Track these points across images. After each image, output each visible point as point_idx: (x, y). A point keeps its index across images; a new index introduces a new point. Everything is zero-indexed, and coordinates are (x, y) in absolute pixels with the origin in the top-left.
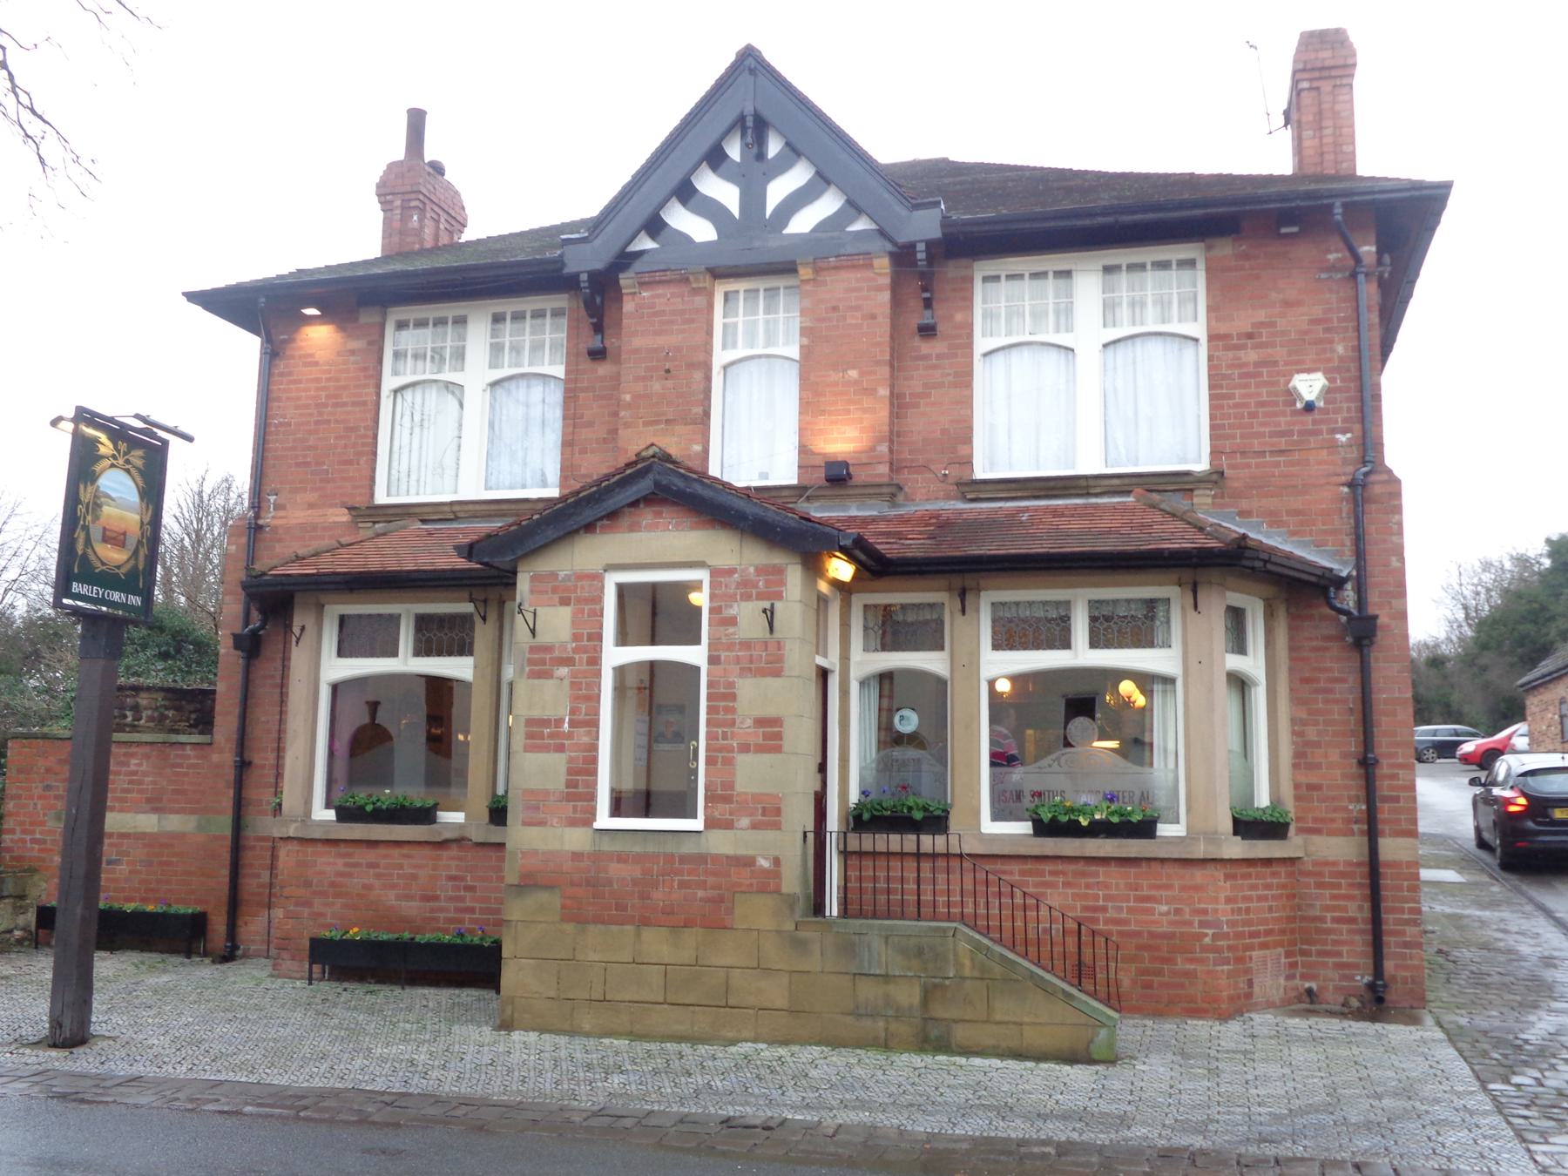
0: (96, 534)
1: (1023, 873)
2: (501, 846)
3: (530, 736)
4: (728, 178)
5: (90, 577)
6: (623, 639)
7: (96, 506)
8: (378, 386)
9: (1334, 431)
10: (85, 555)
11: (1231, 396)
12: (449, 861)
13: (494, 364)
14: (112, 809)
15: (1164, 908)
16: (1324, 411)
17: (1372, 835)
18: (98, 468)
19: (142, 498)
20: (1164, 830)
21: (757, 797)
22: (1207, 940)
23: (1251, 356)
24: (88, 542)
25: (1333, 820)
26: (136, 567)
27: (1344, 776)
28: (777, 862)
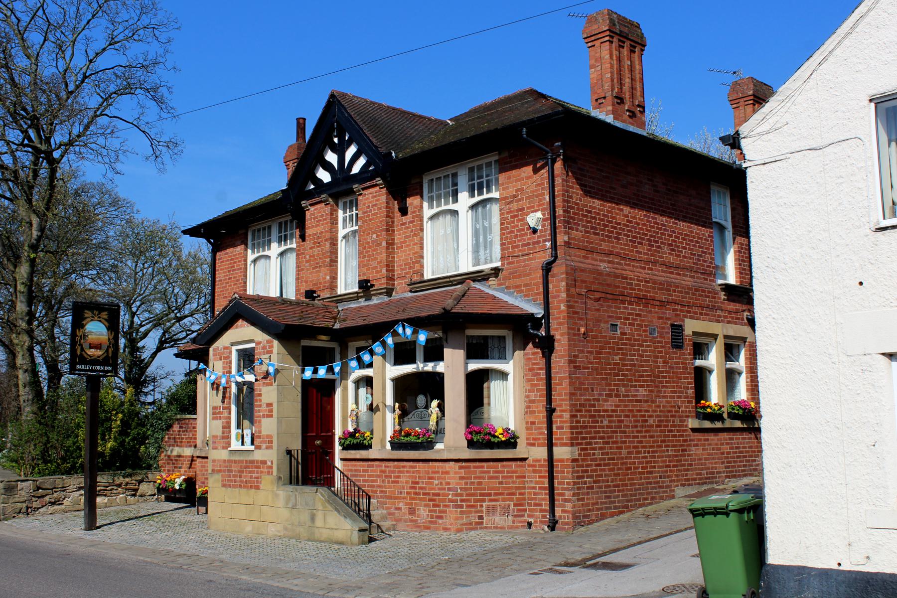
0: (86, 346)
1: (517, 466)
3: (214, 413)
5: (83, 360)
7: (85, 336)
8: (246, 260)
9: (545, 241)
10: (81, 354)
12: (377, 467)
13: (473, 196)
14: (544, 460)
16: (542, 231)
17: (550, 446)
18: (84, 322)
19: (108, 329)
22: (450, 497)
23: (514, 206)
24: (82, 350)
25: (539, 439)
26: (108, 355)
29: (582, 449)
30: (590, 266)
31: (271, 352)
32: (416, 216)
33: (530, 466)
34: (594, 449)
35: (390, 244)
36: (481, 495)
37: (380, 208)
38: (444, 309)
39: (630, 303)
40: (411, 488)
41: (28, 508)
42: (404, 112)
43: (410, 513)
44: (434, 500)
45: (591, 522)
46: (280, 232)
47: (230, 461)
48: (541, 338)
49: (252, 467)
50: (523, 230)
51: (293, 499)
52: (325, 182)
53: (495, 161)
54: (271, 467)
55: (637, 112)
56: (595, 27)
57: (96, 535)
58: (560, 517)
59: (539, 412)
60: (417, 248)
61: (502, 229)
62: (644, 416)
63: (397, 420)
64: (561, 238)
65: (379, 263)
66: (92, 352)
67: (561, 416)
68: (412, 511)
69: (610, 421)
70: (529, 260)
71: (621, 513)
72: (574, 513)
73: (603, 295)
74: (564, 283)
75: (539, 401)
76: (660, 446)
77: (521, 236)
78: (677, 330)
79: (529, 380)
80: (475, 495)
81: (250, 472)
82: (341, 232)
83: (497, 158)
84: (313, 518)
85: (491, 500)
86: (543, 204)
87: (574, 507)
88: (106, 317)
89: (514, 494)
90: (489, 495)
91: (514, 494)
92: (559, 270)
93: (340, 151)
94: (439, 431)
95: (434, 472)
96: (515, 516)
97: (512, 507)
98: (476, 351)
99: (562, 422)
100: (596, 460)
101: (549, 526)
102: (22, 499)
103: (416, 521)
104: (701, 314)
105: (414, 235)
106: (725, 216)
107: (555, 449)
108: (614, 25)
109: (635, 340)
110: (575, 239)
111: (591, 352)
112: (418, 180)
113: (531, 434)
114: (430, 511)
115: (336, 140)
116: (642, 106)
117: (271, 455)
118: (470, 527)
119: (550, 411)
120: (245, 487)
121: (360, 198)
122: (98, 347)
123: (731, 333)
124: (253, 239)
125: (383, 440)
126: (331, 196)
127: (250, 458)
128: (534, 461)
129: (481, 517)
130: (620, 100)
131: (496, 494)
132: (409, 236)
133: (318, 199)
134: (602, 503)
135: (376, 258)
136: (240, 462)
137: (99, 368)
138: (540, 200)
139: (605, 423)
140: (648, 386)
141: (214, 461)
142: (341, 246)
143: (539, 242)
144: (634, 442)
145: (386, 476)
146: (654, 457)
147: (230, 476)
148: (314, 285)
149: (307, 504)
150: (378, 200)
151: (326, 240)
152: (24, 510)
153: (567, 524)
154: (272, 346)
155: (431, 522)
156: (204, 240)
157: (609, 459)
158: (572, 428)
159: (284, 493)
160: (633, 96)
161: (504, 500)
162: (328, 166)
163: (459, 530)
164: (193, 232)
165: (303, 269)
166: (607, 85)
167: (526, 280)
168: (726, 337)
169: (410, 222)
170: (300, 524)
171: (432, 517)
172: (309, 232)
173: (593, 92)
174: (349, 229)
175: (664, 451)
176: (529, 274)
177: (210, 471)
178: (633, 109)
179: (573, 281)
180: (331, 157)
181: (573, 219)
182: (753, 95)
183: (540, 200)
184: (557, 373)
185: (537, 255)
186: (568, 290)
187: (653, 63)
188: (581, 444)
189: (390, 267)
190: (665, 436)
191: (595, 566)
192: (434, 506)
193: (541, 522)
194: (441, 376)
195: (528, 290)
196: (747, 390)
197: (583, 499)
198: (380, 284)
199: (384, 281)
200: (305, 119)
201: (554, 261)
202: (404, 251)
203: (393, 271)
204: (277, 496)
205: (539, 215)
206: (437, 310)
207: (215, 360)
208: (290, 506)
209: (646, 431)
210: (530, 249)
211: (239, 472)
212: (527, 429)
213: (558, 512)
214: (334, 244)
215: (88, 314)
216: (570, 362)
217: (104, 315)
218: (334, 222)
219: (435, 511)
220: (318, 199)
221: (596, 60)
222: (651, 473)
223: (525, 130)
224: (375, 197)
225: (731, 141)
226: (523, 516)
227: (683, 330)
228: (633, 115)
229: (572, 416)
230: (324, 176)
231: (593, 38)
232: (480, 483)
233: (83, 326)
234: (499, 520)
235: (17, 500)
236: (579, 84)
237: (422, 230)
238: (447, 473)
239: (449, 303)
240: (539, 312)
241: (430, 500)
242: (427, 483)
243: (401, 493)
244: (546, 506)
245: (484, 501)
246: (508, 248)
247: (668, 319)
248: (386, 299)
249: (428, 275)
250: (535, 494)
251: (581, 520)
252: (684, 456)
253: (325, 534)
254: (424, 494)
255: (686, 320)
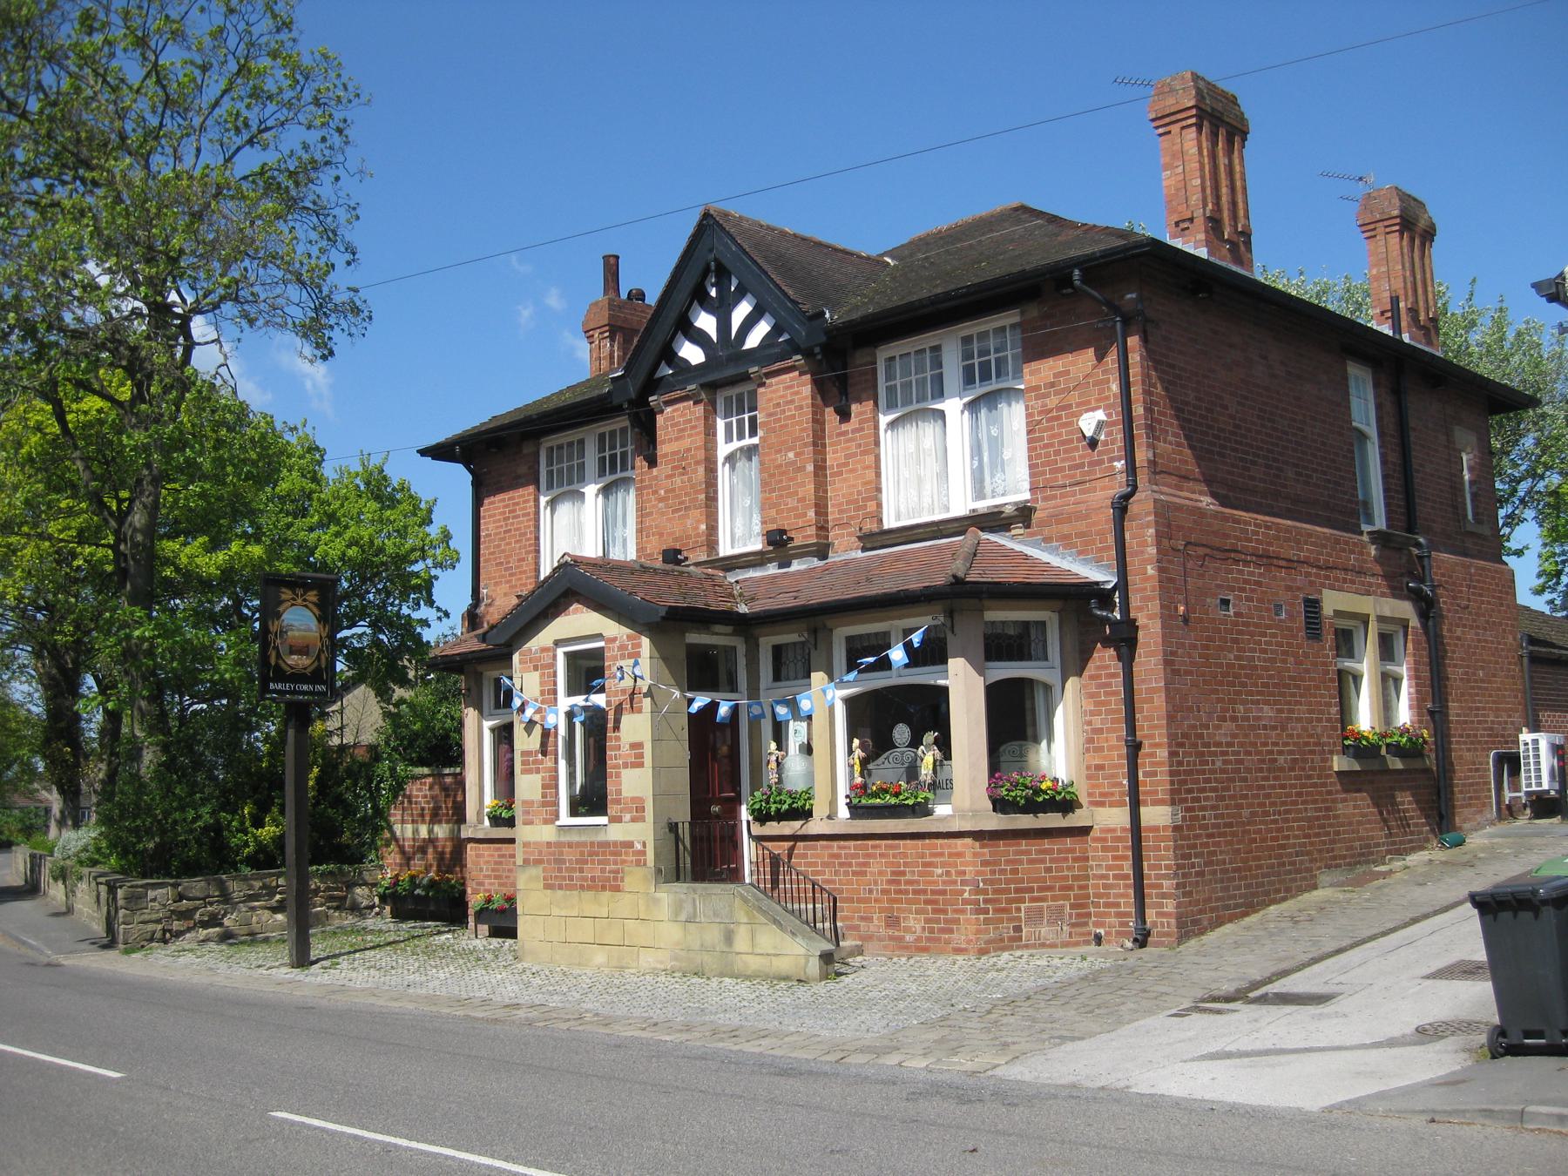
2: (512, 841)
4: (710, 311)
5: (281, 675)
6: (571, 692)
7: (283, 633)
9: (1112, 460)
11: (1042, 439)
14: (1123, 830)
15: (939, 871)
16: (1105, 443)
20: (942, 810)
21: (634, 799)
22: (966, 895)
23: (1052, 402)
24: (279, 656)
25: (1112, 794)
27: (1119, 756)
28: (644, 845)
29: (1188, 809)
30: (1187, 502)
31: (638, 655)
32: (866, 420)
33: (1096, 840)
34: (1203, 808)
35: (820, 468)
36: (1017, 891)
37: (801, 408)
38: (954, 576)
39: (1247, 564)
40: (890, 882)
41: (164, 931)
42: (819, 244)
43: (888, 926)
44: (935, 902)
45: (1202, 932)
46: (602, 449)
47: (559, 844)
48: (1114, 624)
49: (604, 854)
50: (1072, 441)
51: (688, 908)
52: (694, 363)
53: (1013, 326)
54: (643, 853)
55: (1241, 244)
56: (1170, 101)
57: (315, 977)
58: (1155, 924)
59: (1111, 748)
60: (870, 474)
61: (1030, 441)
62: (1271, 752)
63: (857, 768)
64: (1142, 455)
65: (802, 500)
66: (293, 660)
67: (1153, 755)
68: (893, 922)
69: (1225, 762)
70: (1082, 492)
71: (1246, 914)
72: (1179, 917)
73: (1208, 551)
74: (1152, 531)
75: (1109, 730)
76: (1295, 803)
77: (1066, 451)
78: (1313, 606)
79: (1091, 696)
80: (1008, 891)
81: (600, 862)
82: (723, 449)
83: (1017, 319)
84: (729, 938)
85: (1033, 900)
86: (1107, 398)
87: (1178, 906)
88: (315, 599)
89: (1070, 888)
90: (1031, 890)
91: (1070, 888)
92: (1142, 505)
93: (722, 312)
94: (940, 786)
95: (932, 855)
96: (1073, 925)
97: (1068, 910)
98: (999, 646)
99: (1153, 764)
100: (1205, 827)
101: (1136, 940)
102: (154, 916)
103: (901, 939)
104: (1345, 581)
105: (864, 453)
106: (1367, 418)
107: (1143, 810)
108: (1203, 98)
109: (1256, 625)
110: (1162, 457)
111: (1194, 647)
112: (869, 359)
113: (1098, 786)
114: (927, 921)
115: (713, 293)
116: (1247, 234)
117: (641, 833)
118: (1000, 945)
119: (1134, 748)
120: (590, 888)
121: (761, 390)
122: (303, 650)
123: (1388, 613)
124: (550, 463)
125: (833, 803)
126: (703, 386)
127: (601, 837)
128: (1102, 831)
129: (1018, 929)
130: (1214, 223)
131: (1041, 889)
132: (855, 455)
133: (679, 394)
134: (1218, 899)
135: (796, 493)
136: (578, 844)
137: (305, 687)
138: (1101, 391)
139: (1219, 764)
140: (1276, 703)
141: (526, 845)
142: (723, 473)
143: (1101, 462)
144: (1258, 796)
145: (841, 865)
146: (1287, 821)
147: (560, 870)
148: (676, 540)
149: (716, 914)
150: (797, 393)
151: (697, 463)
152: (158, 935)
153: (1167, 934)
154: (639, 645)
155: (929, 939)
156: (460, 467)
157: (1226, 825)
158: (1171, 773)
159: (668, 896)
160: (1234, 217)
161: (1054, 898)
162: (699, 338)
163: (982, 952)
164: (439, 452)
165: (651, 514)
166: (1195, 198)
167: (1081, 526)
168: (1381, 619)
169: (854, 431)
170: (704, 948)
171: (932, 931)
172: (663, 449)
173: (1172, 211)
174: (736, 444)
175: (1299, 811)
176: (1087, 517)
177: (519, 861)
178: (1235, 238)
179: (1166, 531)
180: (706, 322)
181: (1160, 422)
182: (1400, 216)
183: (1101, 391)
184: (1143, 681)
185: (1098, 484)
186: (1158, 544)
187: (1256, 156)
188: (1186, 800)
189: (821, 508)
190: (1303, 786)
191: (1263, 1000)
192: (935, 911)
193: (1118, 933)
194: (945, 690)
195: (1086, 544)
196: (1411, 707)
197: (1190, 893)
198: (804, 536)
199: (812, 531)
200: (617, 258)
201: (1132, 494)
202: (845, 480)
203: (826, 514)
204: (656, 901)
205: (1100, 415)
206: (940, 580)
207: (523, 670)
208: (683, 917)
209: (1275, 778)
210: (1083, 474)
211: (577, 862)
212: (1089, 777)
213: (1151, 915)
214: (711, 471)
215: (286, 594)
216: (1167, 663)
217: (312, 596)
218: (710, 432)
219: (938, 921)
220: (679, 394)
221: (1174, 156)
222: (1283, 847)
223: (1077, 272)
224: (789, 393)
225: (1554, 290)
226: (1086, 924)
227: (1321, 608)
228: (1234, 247)
229: (1172, 754)
230: (692, 353)
231: (1167, 120)
232: (1015, 871)
233: (279, 615)
234: (1045, 931)
235: (146, 917)
236: (1144, 193)
237: (877, 443)
238: (960, 855)
239: (958, 567)
240: (1103, 576)
241: (927, 902)
242: (921, 874)
243: (871, 891)
244: (1128, 904)
245: (1022, 901)
246: (1044, 473)
247: (1299, 589)
248: (815, 562)
249: (890, 522)
250: (1105, 886)
251: (1189, 927)
252: (1328, 818)
253: (754, 963)
254: (916, 892)
255: (1325, 591)
